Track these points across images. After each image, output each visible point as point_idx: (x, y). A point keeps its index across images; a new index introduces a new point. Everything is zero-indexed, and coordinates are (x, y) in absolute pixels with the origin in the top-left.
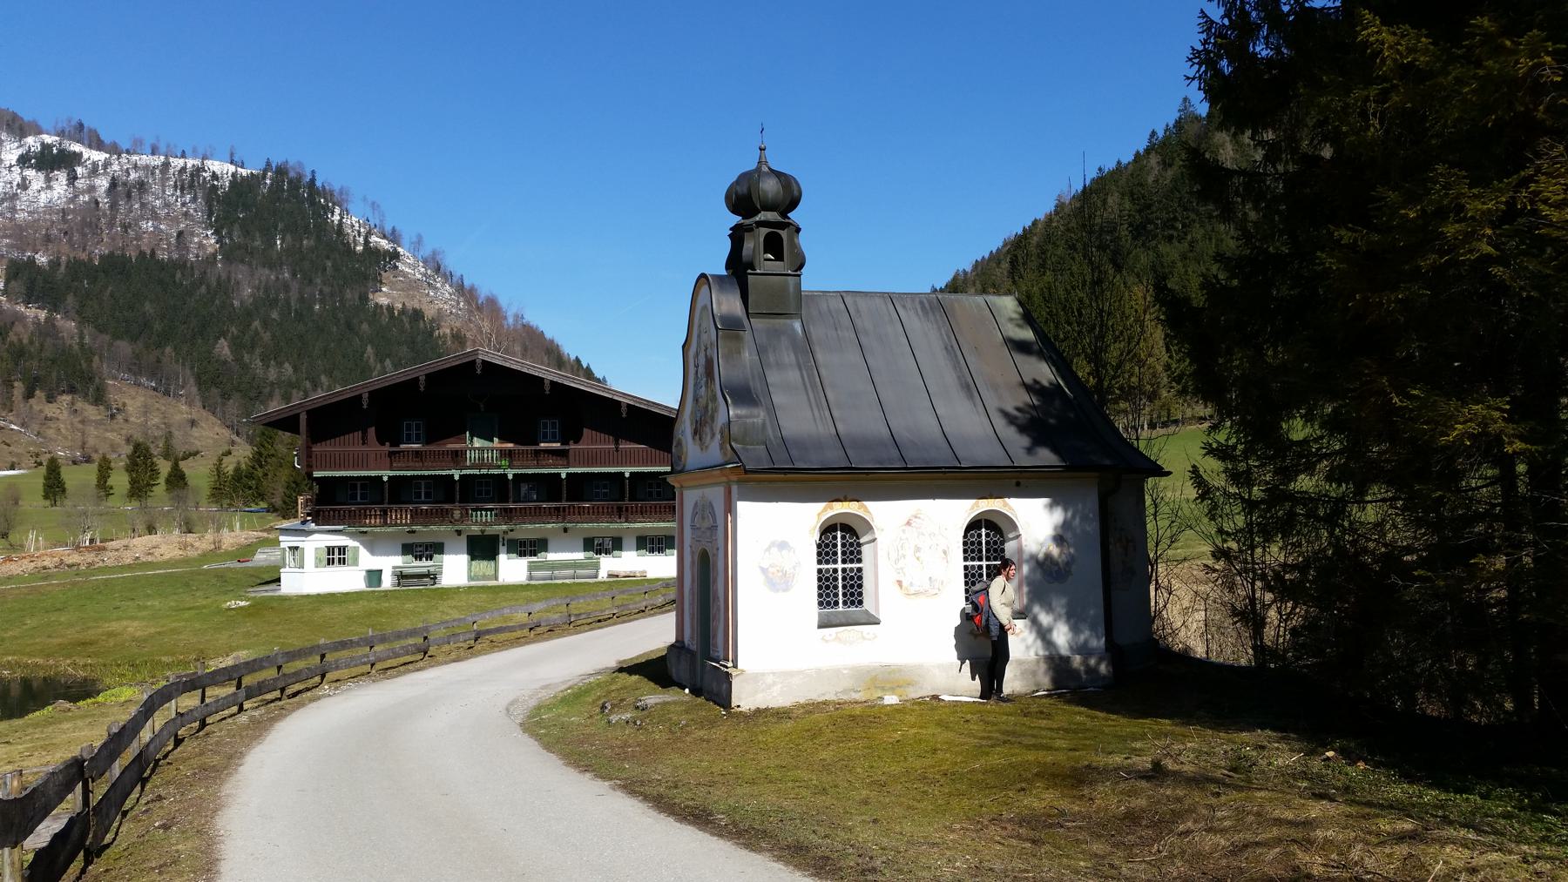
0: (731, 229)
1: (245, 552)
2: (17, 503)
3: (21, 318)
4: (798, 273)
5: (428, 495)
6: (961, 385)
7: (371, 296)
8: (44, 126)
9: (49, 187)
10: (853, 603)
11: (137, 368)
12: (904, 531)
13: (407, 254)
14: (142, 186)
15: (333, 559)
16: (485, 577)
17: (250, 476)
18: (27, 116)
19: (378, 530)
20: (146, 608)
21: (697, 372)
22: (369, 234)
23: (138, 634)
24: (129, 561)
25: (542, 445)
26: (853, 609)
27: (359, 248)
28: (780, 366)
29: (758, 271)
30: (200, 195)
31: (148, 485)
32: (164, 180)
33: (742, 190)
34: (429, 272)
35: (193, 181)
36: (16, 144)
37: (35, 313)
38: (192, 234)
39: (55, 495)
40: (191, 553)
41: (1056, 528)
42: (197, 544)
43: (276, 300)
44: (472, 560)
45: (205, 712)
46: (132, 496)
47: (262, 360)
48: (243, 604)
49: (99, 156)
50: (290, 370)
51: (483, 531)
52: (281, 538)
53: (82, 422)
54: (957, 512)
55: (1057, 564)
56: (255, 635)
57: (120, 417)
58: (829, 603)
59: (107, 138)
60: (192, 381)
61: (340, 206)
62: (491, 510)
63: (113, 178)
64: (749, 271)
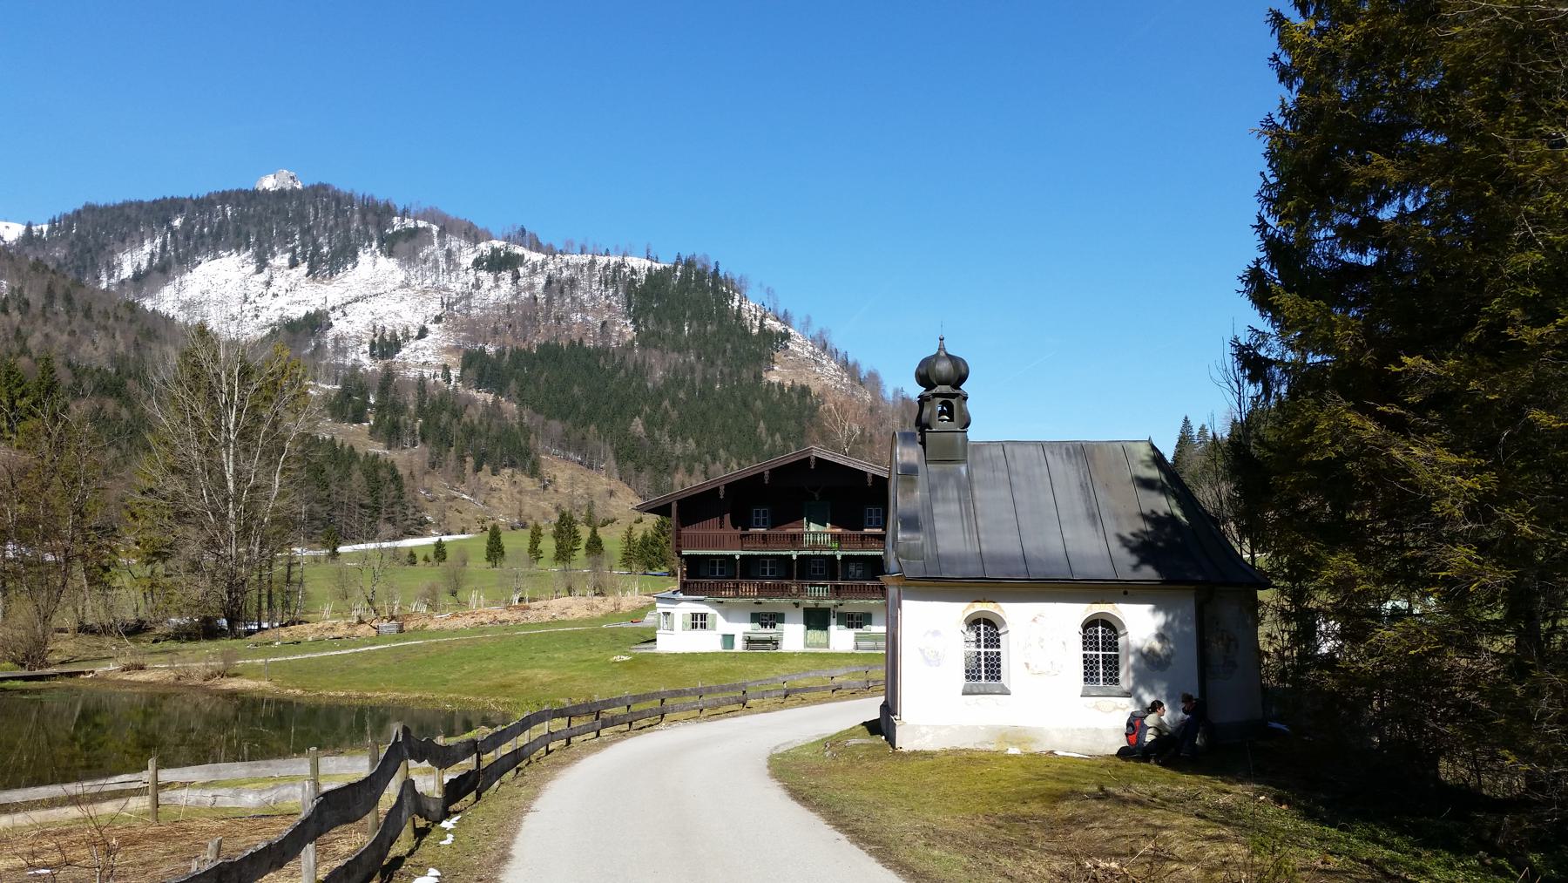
1: (637, 614)
2: (465, 564)
3: (471, 401)
5: (772, 572)
6: (1089, 515)
7: (764, 375)
8: (494, 233)
9: (497, 286)
10: (993, 678)
11: (566, 444)
13: (797, 334)
14: (572, 282)
16: (819, 645)
17: (655, 543)
18: (480, 224)
19: (730, 600)
20: (554, 659)
22: (764, 317)
23: (546, 679)
24: (547, 619)
25: (866, 530)
26: (993, 682)
27: (755, 331)
28: (945, 500)
30: (620, 289)
31: (572, 550)
32: (591, 276)
33: (923, 371)
34: (816, 350)
35: (615, 276)
36: (472, 250)
37: (484, 397)
38: (614, 324)
39: (495, 557)
40: (597, 614)
41: (1158, 629)
42: (601, 606)
43: (684, 381)
44: (808, 629)
45: (570, 734)
46: (558, 559)
47: (670, 436)
48: (625, 658)
49: (537, 257)
50: (694, 445)
51: (817, 605)
52: (658, 605)
53: (520, 492)
54: (1076, 613)
55: (1158, 656)
56: (631, 684)
57: (550, 488)
58: (974, 677)
59: (544, 241)
60: (611, 456)
61: (739, 293)
62: (823, 586)
63: (549, 277)
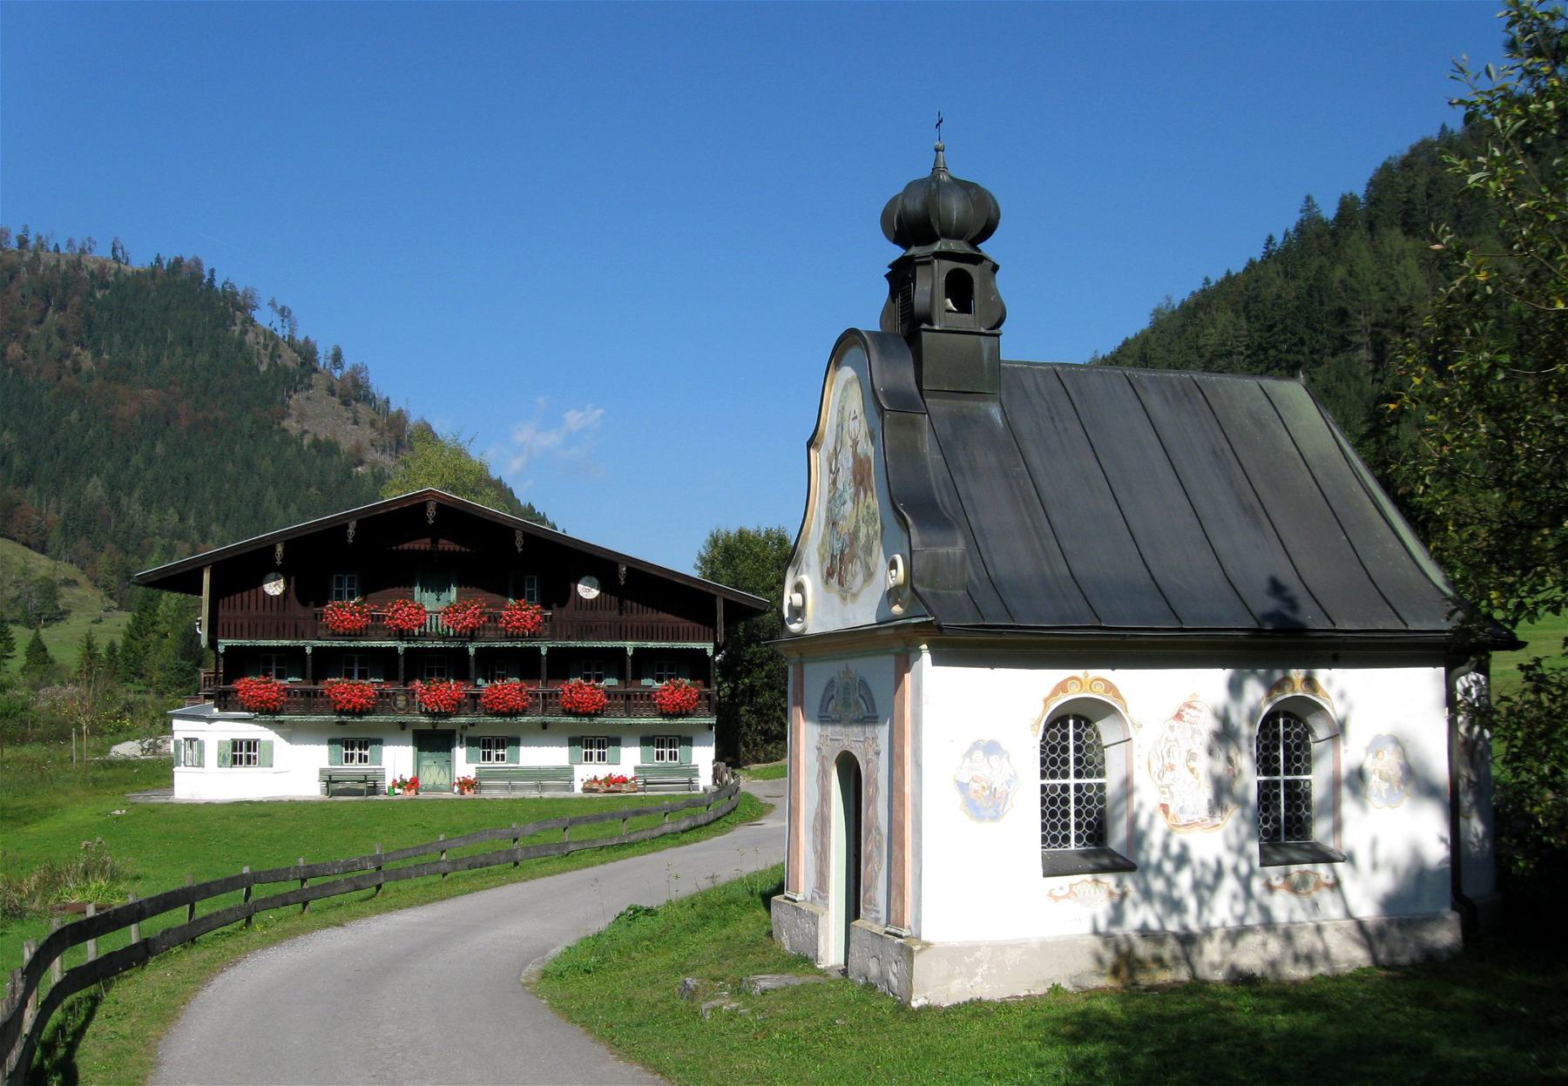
0: (890, 267)
4: (996, 331)
12: (1171, 728)
15: (241, 756)
21: (834, 482)
29: (937, 327)
33: (915, 205)
58: (1054, 839)
64: (925, 326)
